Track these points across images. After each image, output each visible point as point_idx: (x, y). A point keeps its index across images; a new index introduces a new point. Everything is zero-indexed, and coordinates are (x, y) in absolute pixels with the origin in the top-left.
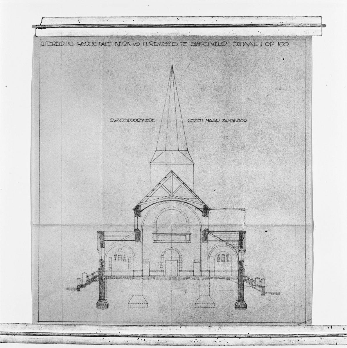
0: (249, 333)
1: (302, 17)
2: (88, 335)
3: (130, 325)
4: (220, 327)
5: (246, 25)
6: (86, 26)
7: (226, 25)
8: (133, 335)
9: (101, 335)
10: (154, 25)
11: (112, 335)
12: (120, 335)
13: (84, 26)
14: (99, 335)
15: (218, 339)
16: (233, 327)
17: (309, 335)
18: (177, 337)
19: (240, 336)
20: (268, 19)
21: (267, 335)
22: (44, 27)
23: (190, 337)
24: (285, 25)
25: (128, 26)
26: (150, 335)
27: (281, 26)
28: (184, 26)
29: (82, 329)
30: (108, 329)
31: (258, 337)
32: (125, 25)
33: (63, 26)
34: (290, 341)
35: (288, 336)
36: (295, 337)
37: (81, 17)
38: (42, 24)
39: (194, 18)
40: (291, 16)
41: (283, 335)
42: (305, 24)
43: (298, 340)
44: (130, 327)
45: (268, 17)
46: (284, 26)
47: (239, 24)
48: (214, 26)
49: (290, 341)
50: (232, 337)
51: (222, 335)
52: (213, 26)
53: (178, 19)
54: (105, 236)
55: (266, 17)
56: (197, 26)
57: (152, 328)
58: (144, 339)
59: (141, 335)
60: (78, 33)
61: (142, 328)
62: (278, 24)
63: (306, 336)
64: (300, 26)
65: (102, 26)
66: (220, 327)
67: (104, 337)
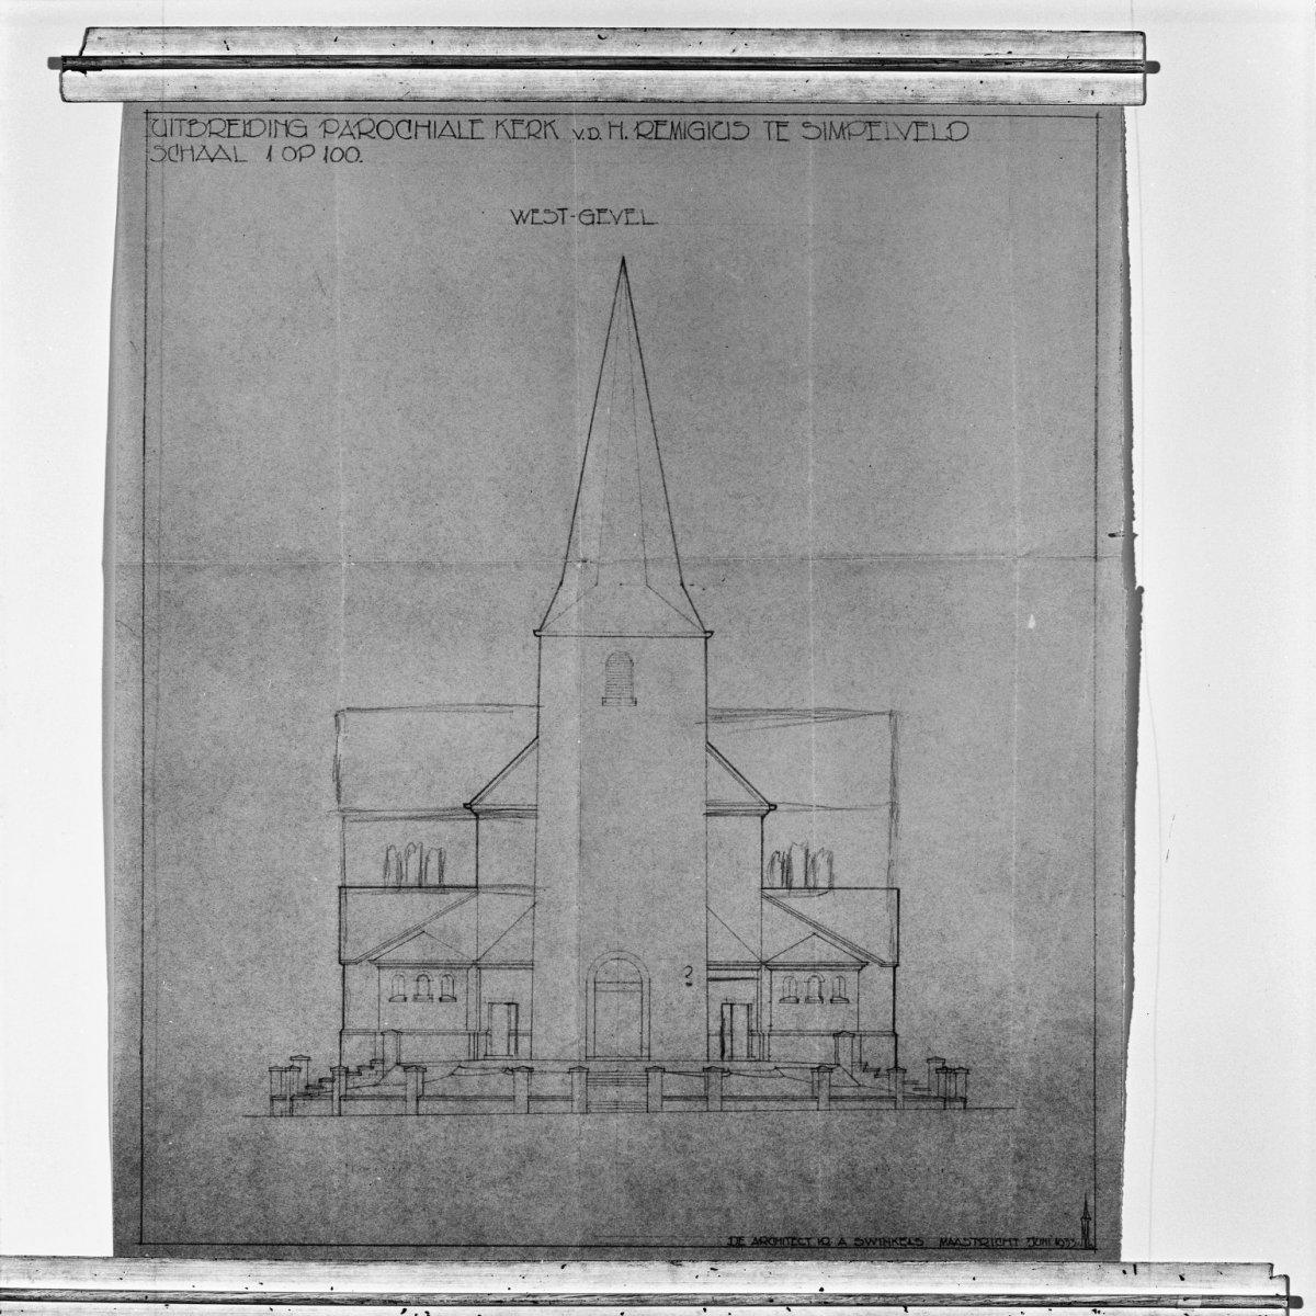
0: (822, 1289)
10: (511, 61)
12: (334, 1297)
13: (247, 62)
18: (551, 1304)
21: (892, 1296)
22: (93, 63)
31: (858, 1305)
38: (85, 54)
41: (949, 1296)
42: (1081, 61)
46: (1003, 66)
50: (758, 1302)
51: (722, 1294)
53: (599, 37)
56: (671, 63)
67: (272, 1307)
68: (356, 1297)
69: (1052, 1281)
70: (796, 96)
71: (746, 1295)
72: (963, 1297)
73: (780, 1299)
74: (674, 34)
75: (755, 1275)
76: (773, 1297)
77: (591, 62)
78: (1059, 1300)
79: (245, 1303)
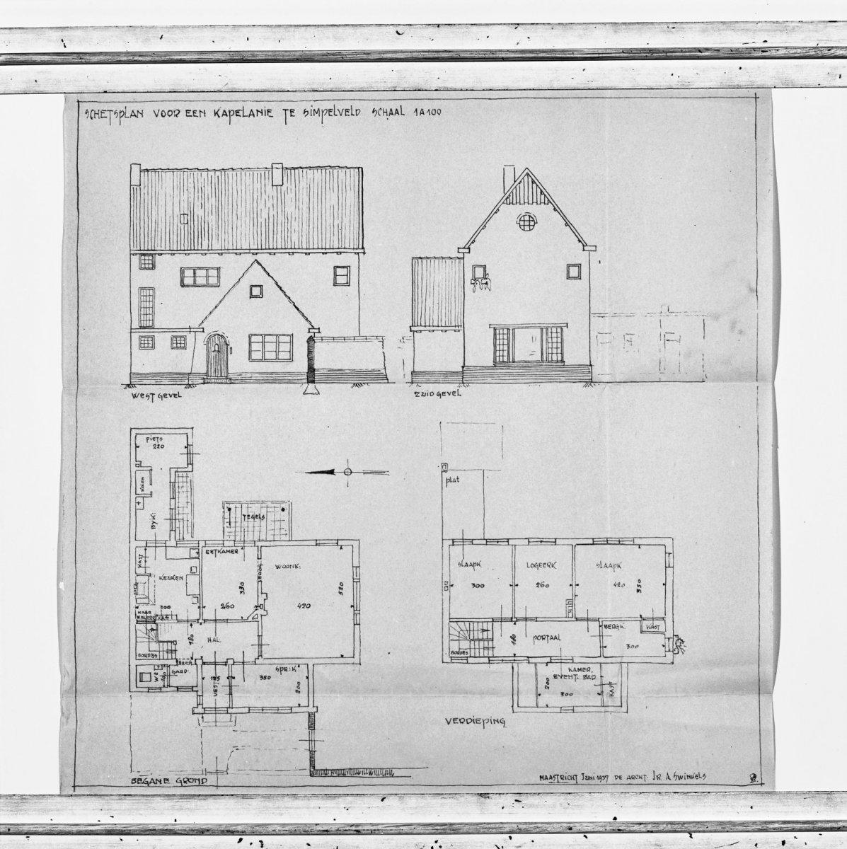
0: (615, 819)
1: (821, 25)
2: (68, 829)
3: (211, 795)
4: (518, 798)
5: (630, 51)
6: (87, 57)
7: (563, 51)
8: (223, 828)
9: (113, 830)
10: (318, 55)
11: (151, 827)
12: (177, 827)
13: (81, 59)
14: (106, 830)
15: (510, 838)
16: (562, 797)
17: (819, 825)
18: (372, 833)
19: (586, 829)
20: (704, 31)
21: (678, 823)
23: (415, 831)
24: (763, 51)
25: (228, 57)
26: (279, 828)
27: (747, 55)
28: (421, 55)
29: (50, 810)
30: (136, 809)
31: (648, 832)
32: (219, 54)
33: (9, 57)
34: (756, 845)
35: (750, 829)
36: (775, 830)
37: (71, 28)
39: (453, 28)
40: (780, 20)
41: (730, 823)
42: (830, 49)
43: (784, 843)
44: (211, 800)
45: (702, 25)
46: (760, 54)
47: (606, 49)
48: (520, 56)
49: (756, 845)
50: (558, 830)
51: (526, 823)
52: (517, 56)
53: (398, 33)
54: (146, 173)
55: (697, 25)
56: (462, 55)
57: (288, 802)
58: (261, 841)
59: (249, 829)
60: (59, 81)
61: (254, 803)
62: (737, 50)
63: (811, 826)
64: (812, 53)
65: (140, 59)
66: (518, 798)
67: (122, 837)
68: (197, 827)
69: (822, 808)
70: (573, 84)
71: (548, 823)
72: (742, 824)
73: (578, 827)
74: (464, 29)
75: (554, 806)
76: (571, 825)
77: (389, 56)
78: (829, 825)
79: (97, 834)
